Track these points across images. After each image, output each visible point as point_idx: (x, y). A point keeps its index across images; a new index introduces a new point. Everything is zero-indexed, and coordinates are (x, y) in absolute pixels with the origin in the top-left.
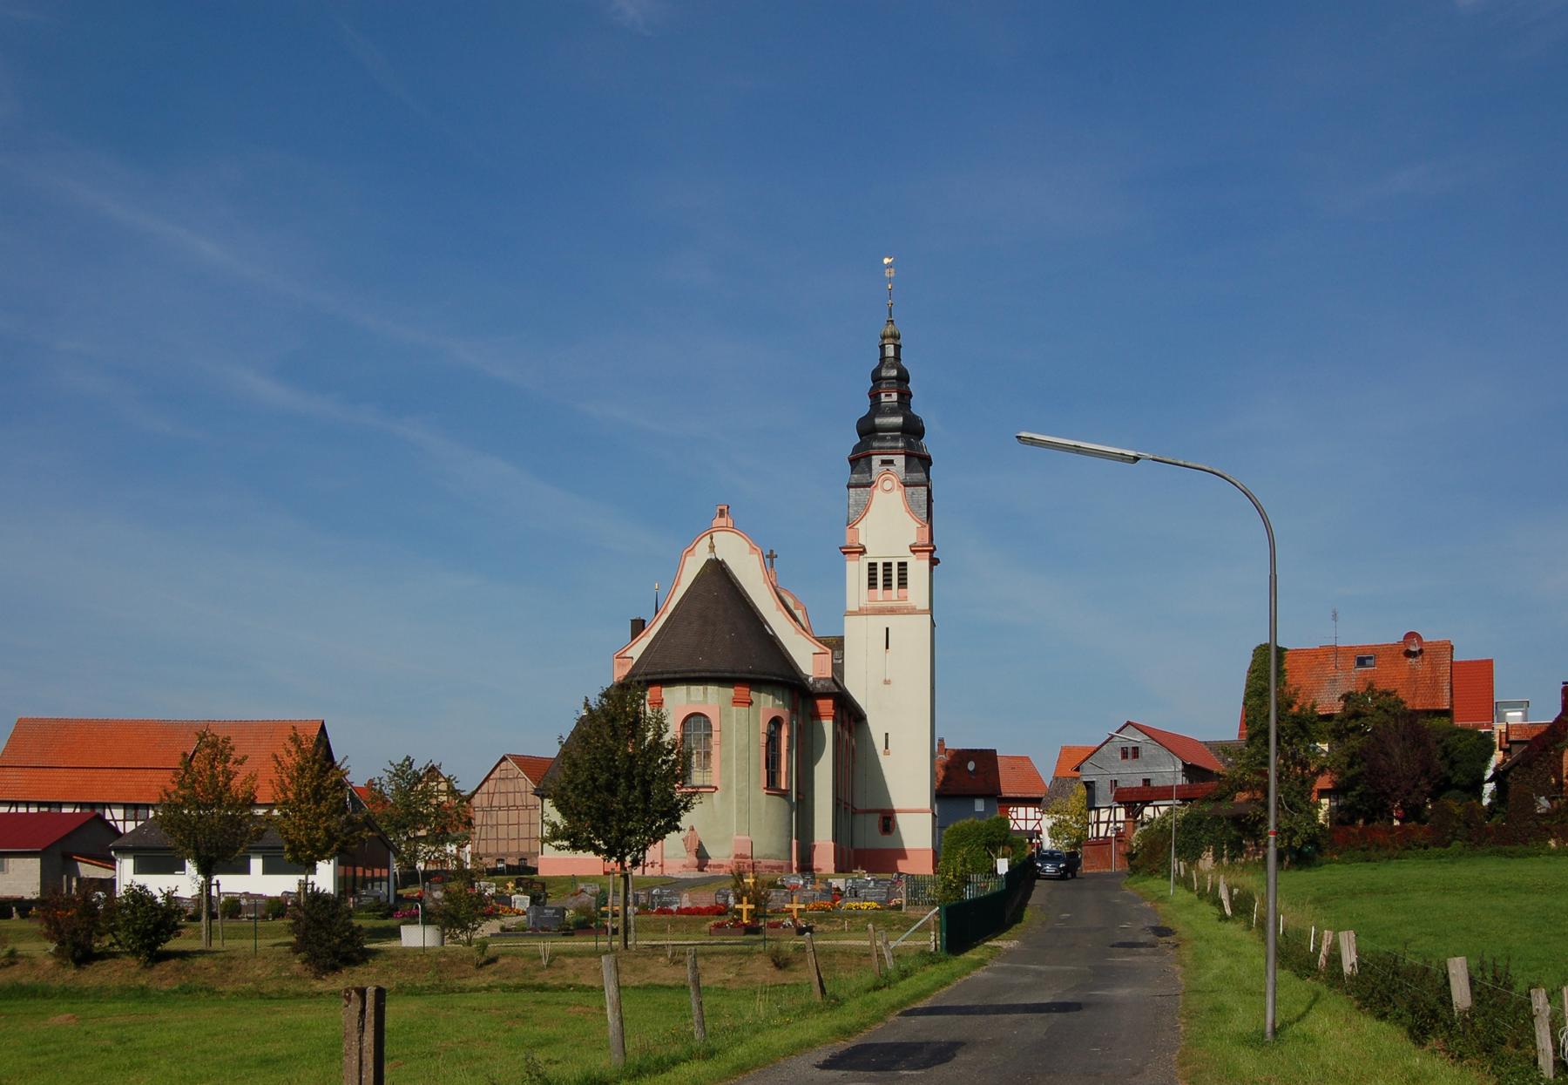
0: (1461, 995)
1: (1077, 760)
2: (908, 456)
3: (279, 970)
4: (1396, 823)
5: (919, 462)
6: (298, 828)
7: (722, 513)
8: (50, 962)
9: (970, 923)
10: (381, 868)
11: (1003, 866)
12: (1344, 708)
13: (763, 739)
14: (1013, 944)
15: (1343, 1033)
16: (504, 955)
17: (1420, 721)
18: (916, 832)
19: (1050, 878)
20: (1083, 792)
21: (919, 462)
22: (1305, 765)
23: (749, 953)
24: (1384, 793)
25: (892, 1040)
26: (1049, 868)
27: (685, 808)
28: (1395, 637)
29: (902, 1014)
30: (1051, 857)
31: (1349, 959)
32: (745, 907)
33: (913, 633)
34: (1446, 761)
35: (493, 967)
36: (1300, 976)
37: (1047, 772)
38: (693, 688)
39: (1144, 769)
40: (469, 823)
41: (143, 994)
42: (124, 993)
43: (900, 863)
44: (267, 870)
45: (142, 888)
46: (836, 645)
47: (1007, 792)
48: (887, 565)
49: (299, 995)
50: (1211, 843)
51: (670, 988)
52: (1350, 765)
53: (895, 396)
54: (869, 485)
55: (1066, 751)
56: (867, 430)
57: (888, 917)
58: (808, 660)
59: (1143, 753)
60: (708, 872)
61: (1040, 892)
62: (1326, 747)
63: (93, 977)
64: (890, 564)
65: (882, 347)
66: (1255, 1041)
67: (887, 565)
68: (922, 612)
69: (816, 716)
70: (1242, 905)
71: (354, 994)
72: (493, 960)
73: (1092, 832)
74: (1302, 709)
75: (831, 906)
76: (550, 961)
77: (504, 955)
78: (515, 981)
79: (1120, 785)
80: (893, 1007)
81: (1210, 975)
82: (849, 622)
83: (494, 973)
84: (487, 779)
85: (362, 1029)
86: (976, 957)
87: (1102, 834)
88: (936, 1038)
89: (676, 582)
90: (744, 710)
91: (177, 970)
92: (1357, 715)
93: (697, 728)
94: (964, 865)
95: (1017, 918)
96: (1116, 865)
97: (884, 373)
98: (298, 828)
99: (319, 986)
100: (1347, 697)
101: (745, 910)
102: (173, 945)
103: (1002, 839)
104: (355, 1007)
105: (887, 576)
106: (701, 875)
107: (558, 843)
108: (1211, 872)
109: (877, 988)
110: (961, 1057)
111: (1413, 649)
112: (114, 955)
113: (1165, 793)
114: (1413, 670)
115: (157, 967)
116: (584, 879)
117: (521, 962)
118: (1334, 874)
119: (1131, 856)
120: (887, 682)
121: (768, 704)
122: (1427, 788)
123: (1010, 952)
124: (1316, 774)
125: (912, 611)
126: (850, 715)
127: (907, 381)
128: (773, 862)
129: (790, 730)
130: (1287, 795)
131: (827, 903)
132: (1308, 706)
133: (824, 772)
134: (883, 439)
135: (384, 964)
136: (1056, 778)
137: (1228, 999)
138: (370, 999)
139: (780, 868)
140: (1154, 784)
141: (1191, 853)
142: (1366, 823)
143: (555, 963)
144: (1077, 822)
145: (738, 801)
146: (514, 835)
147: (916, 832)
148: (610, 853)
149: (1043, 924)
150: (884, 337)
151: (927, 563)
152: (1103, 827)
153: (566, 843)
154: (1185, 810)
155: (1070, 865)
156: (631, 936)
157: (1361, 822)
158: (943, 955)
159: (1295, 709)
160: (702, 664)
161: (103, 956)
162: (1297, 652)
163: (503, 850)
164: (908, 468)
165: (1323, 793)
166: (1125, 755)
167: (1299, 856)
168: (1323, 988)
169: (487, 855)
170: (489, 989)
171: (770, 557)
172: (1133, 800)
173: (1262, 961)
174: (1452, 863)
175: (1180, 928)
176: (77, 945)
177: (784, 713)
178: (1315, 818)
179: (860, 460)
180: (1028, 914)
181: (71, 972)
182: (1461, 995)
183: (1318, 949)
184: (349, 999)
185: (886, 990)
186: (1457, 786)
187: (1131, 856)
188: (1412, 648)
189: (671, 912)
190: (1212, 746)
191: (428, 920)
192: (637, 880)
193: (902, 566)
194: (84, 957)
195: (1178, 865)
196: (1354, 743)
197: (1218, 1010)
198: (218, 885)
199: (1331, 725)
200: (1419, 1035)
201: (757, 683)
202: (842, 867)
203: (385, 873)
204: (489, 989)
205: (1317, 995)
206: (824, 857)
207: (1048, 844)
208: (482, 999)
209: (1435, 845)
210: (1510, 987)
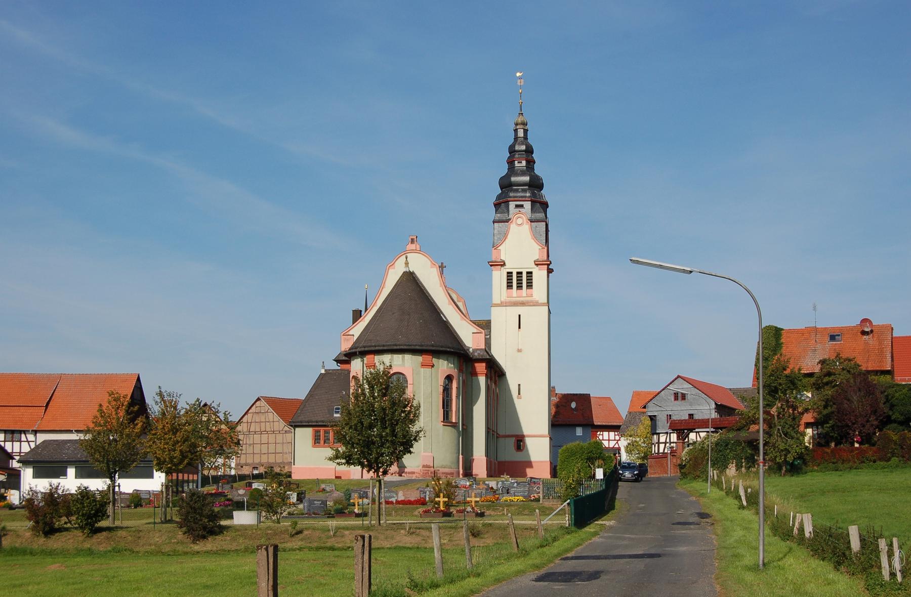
0: (855, 545)
1: (643, 401)
3: (170, 538)
4: (857, 445)
5: (540, 205)
6: (163, 450)
7: (412, 241)
8: (28, 534)
11: (599, 474)
12: (821, 369)
13: (441, 389)
14: (612, 523)
15: (801, 566)
16: (307, 529)
17: (872, 378)
18: (539, 450)
19: (627, 481)
20: (648, 422)
21: (540, 205)
22: (794, 408)
24: (847, 426)
26: (627, 474)
28: (855, 322)
30: (629, 467)
31: (808, 530)
32: (442, 500)
33: (536, 318)
34: (888, 405)
35: (300, 536)
36: (783, 540)
38: (395, 356)
39: (689, 408)
41: (90, 552)
42: (79, 552)
44: (78, 476)
45: (86, 488)
46: (485, 326)
47: (597, 422)
49: (186, 553)
50: (734, 458)
51: (410, 549)
52: (825, 407)
53: (524, 163)
54: (507, 221)
55: (636, 394)
56: (506, 185)
57: (529, 506)
58: (469, 337)
59: (689, 397)
60: (405, 477)
61: (623, 489)
62: (810, 395)
63: (56, 542)
64: (521, 273)
65: (516, 131)
66: (754, 568)
68: (542, 305)
69: (474, 374)
70: (753, 499)
72: (300, 532)
73: (654, 449)
74: (792, 371)
75: (493, 499)
77: (307, 529)
78: (316, 544)
79: (674, 418)
80: (556, 556)
81: (732, 540)
82: (494, 310)
83: (302, 540)
84: (246, 413)
87: (661, 451)
89: (382, 287)
90: (428, 370)
91: (108, 538)
92: (829, 374)
95: (612, 507)
96: (671, 472)
97: (517, 148)
98: (163, 450)
99: (196, 548)
100: (822, 362)
101: (441, 501)
102: (103, 524)
103: (597, 454)
104: (360, 543)
105: (519, 280)
106: (400, 479)
107: (338, 461)
108: (734, 477)
109: (542, 546)
111: (866, 330)
112: (67, 529)
113: (703, 424)
114: (866, 344)
115: (95, 537)
116: (323, 481)
117: (317, 533)
118: (814, 479)
119: (682, 467)
120: (519, 351)
121: (444, 367)
122: (876, 423)
123: (611, 527)
124: (802, 414)
125: (536, 304)
126: (496, 372)
127: (532, 152)
128: (447, 470)
129: (458, 383)
130: (783, 427)
131: (490, 497)
132: (796, 370)
134: (517, 191)
136: (630, 413)
137: (741, 551)
138: (367, 540)
139: (452, 474)
140: (696, 417)
141: (721, 464)
142: (836, 445)
144: (644, 442)
147: (539, 450)
148: (370, 468)
149: (628, 511)
150: (517, 124)
152: (662, 446)
153: (344, 461)
154: (716, 437)
155: (641, 472)
156: (383, 518)
157: (833, 445)
158: (573, 528)
159: (787, 372)
160: (401, 341)
161: (60, 530)
162: (790, 331)
163: (257, 461)
165: (808, 425)
166: (676, 398)
167: (794, 466)
168: (794, 546)
169: (246, 465)
170: (300, 549)
171: (442, 267)
172: (682, 428)
173: (757, 524)
174: (892, 472)
175: (714, 513)
176: (45, 523)
178: (802, 443)
180: (617, 504)
181: (42, 540)
182: (855, 545)
183: (794, 525)
186: (895, 421)
187: (682, 467)
188: (865, 329)
189: (392, 503)
190: (735, 391)
191: (250, 507)
192: (386, 483)
193: (530, 274)
194: (50, 531)
195: (713, 473)
196: (827, 392)
197: (735, 556)
198: (119, 486)
199: (812, 380)
200: (837, 565)
201: (437, 353)
202: (490, 475)
203: (195, 477)
204: (300, 549)
205: (791, 549)
206: (480, 467)
207: (624, 457)
208: (300, 555)
209: (880, 460)
210: (412, 422)
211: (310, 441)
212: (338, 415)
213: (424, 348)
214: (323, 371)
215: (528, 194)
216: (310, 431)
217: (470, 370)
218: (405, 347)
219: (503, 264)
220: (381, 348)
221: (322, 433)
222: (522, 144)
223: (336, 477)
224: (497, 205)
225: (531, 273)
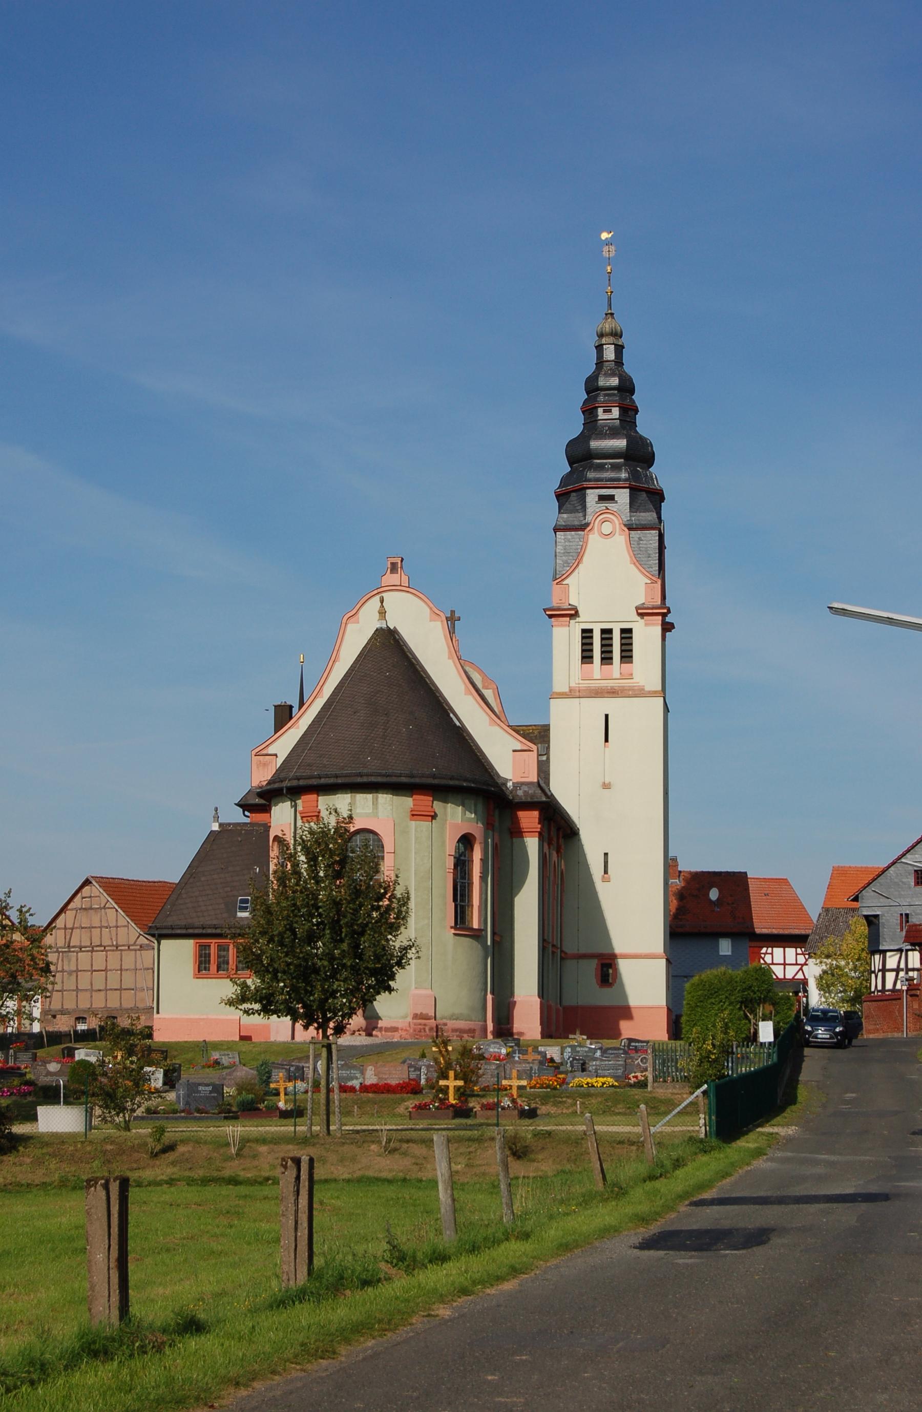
5: (648, 497)
7: (394, 568)
9: (743, 1104)
11: (766, 1032)
13: (450, 863)
14: (791, 1131)
18: (645, 984)
19: (822, 1046)
20: (863, 929)
23: (479, 1140)
25: (695, 1227)
26: (822, 1033)
27: (399, 964)
29: (691, 1204)
30: (824, 1017)
33: (640, 721)
35: (171, 1156)
37: (814, 904)
40: (46, 970)
43: (624, 1025)
46: (538, 736)
47: (761, 928)
48: (607, 633)
51: (390, 1181)
53: (616, 412)
54: (583, 527)
56: (580, 456)
57: (625, 1095)
58: (507, 759)
61: (813, 1064)
64: (610, 631)
65: (599, 348)
68: (652, 694)
69: (517, 832)
71: (290, 1162)
72: (171, 1148)
75: (554, 1084)
76: (240, 1149)
78: (199, 1173)
79: (914, 920)
82: (556, 706)
83: (173, 1163)
84: (63, 910)
85: (298, 1193)
86: (752, 1145)
87: (889, 986)
88: (741, 1225)
89: (333, 658)
90: (425, 825)
94: (726, 1033)
95: (791, 1100)
97: (602, 382)
101: (452, 1086)
103: (764, 993)
104: (291, 1173)
105: (607, 646)
109: (652, 1178)
110: (775, 1241)
116: (217, 1046)
120: (606, 786)
121: (456, 818)
123: (789, 1140)
125: (639, 693)
126: (560, 830)
127: (632, 391)
128: (462, 1024)
129: (485, 852)
131: (548, 1078)
133: (527, 905)
134: (601, 468)
135: (38, 1152)
136: (826, 910)
139: (471, 1031)
143: (246, 1151)
144: (855, 969)
146: (99, 984)
147: (645, 984)
148: (309, 1020)
150: (601, 335)
151: (659, 629)
152: (890, 977)
153: (257, 1006)
155: (848, 1030)
156: (335, 1119)
158: (714, 1141)
160: (372, 766)
163: (84, 1004)
164: (634, 505)
169: (63, 1012)
170: (171, 1182)
171: (452, 619)
177: (477, 829)
180: (802, 1093)
184: (285, 1167)
185: (663, 1180)
189: (352, 1089)
192: (340, 1049)
193: (627, 633)
201: (442, 790)
204: (171, 1182)
207: (815, 998)
208: (168, 1194)
212: (246, 914)
213: (417, 780)
214: (215, 827)
215: (624, 475)
216: (188, 946)
219: (574, 614)
220: (332, 781)
221: (213, 951)
222: (613, 375)
224: (562, 497)
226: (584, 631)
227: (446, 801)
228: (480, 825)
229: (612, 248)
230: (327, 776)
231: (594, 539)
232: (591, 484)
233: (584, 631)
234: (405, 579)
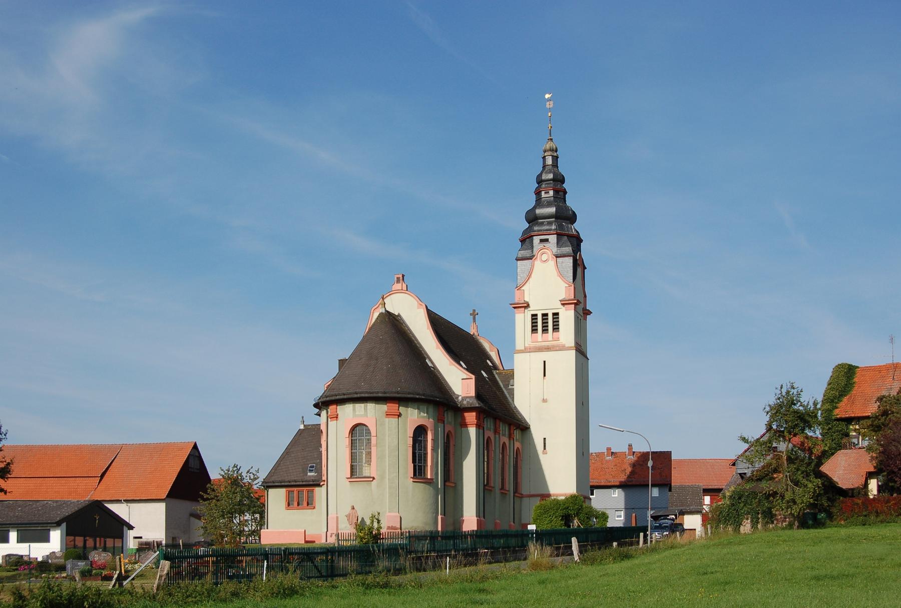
2: (559, 236)
7: (398, 280)
10: (114, 538)
33: (564, 364)
44: (20, 540)
50: (748, 513)
53: (551, 193)
54: (530, 258)
56: (532, 218)
64: (546, 315)
65: (544, 158)
67: (545, 315)
68: (569, 349)
69: (464, 425)
82: (517, 357)
90: (394, 420)
93: (361, 435)
97: (544, 177)
105: (545, 323)
120: (544, 401)
121: (413, 416)
125: (562, 348)
134: (542, 224)
145: (390, 488)
153: (642, 534)
160: (364, 388)
164: (559, 244)
179: (526, 240)
193: (556, 315)
211: (284, 503)
212: (312, 474)
213: (388, 395)
214: (302, 427)
215: (553, 227)
216: (282, 492)
217: (459, 420)
218: (367, 395)
219: (527, 306)
220: (342, 397)
221: (295, 494)
222: (550, 172)
223: (306, 542)
224: (523, 241)
225: (557, 314)
226: (533, 315)
227: (407, 407)
228: (431, 420)
229: (552, 102)
230: (339, 395)
231: (537, 263)
232: (536, 233)
233: (533, 315)
234: (404, 286)
